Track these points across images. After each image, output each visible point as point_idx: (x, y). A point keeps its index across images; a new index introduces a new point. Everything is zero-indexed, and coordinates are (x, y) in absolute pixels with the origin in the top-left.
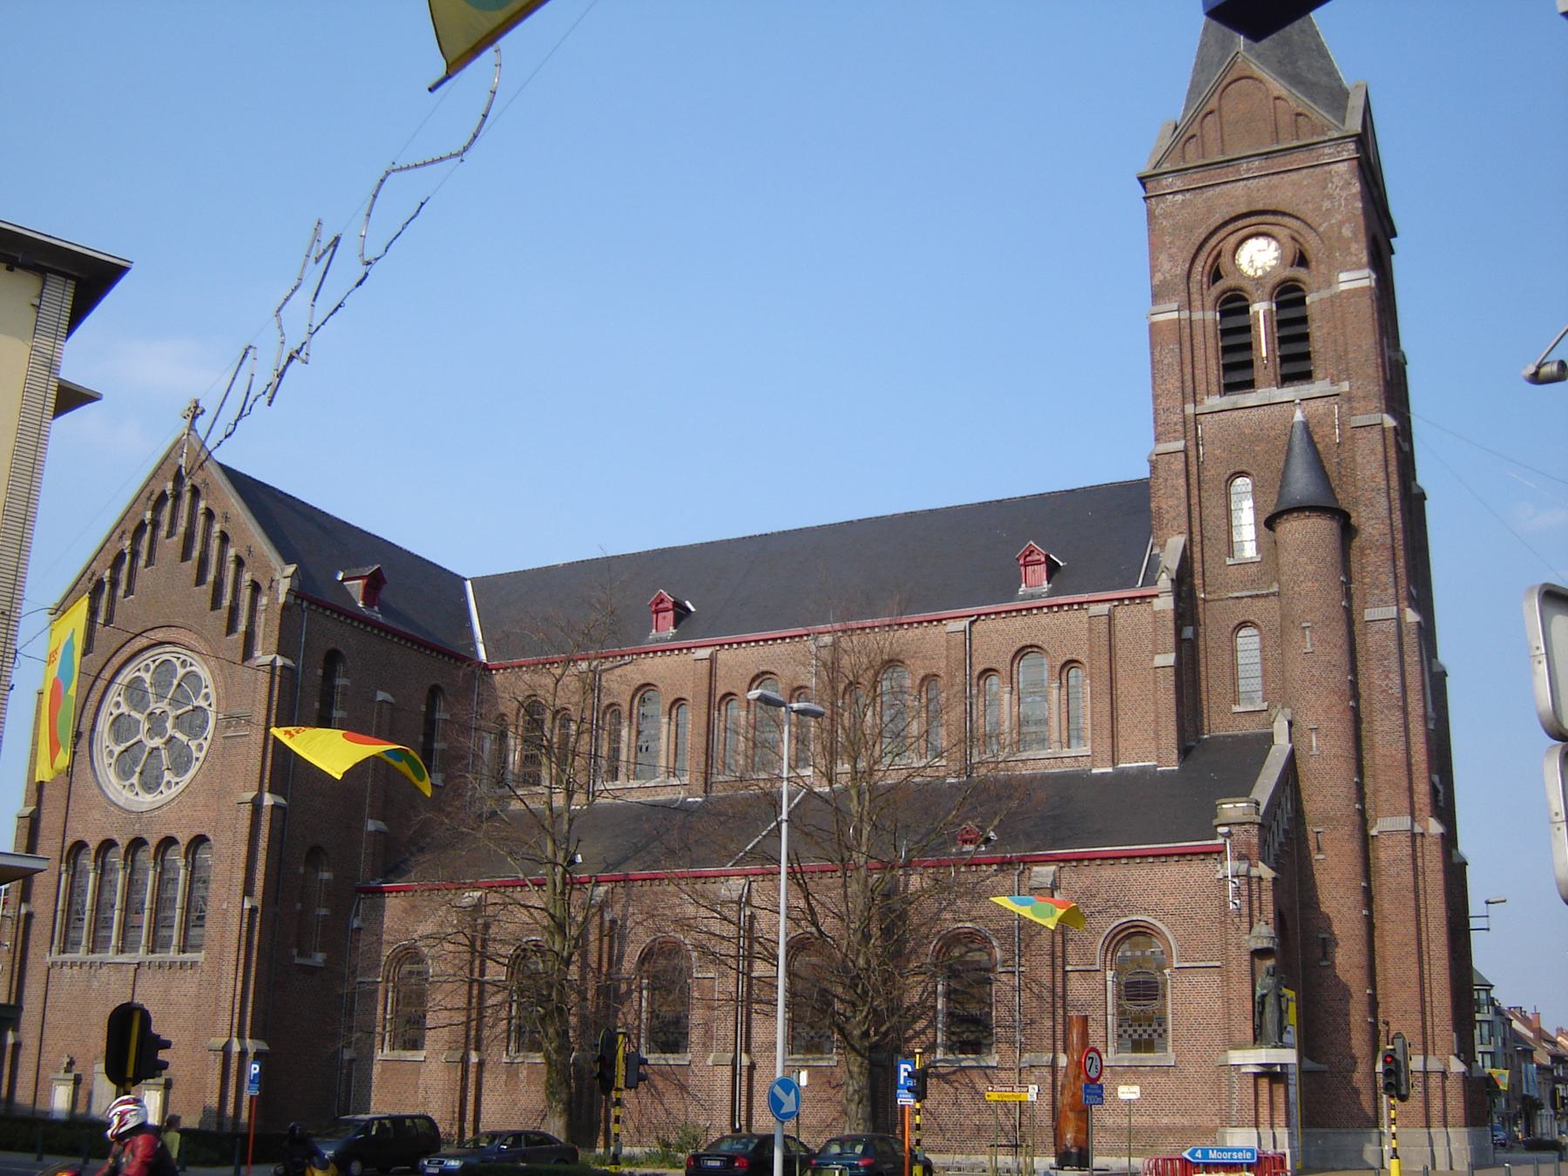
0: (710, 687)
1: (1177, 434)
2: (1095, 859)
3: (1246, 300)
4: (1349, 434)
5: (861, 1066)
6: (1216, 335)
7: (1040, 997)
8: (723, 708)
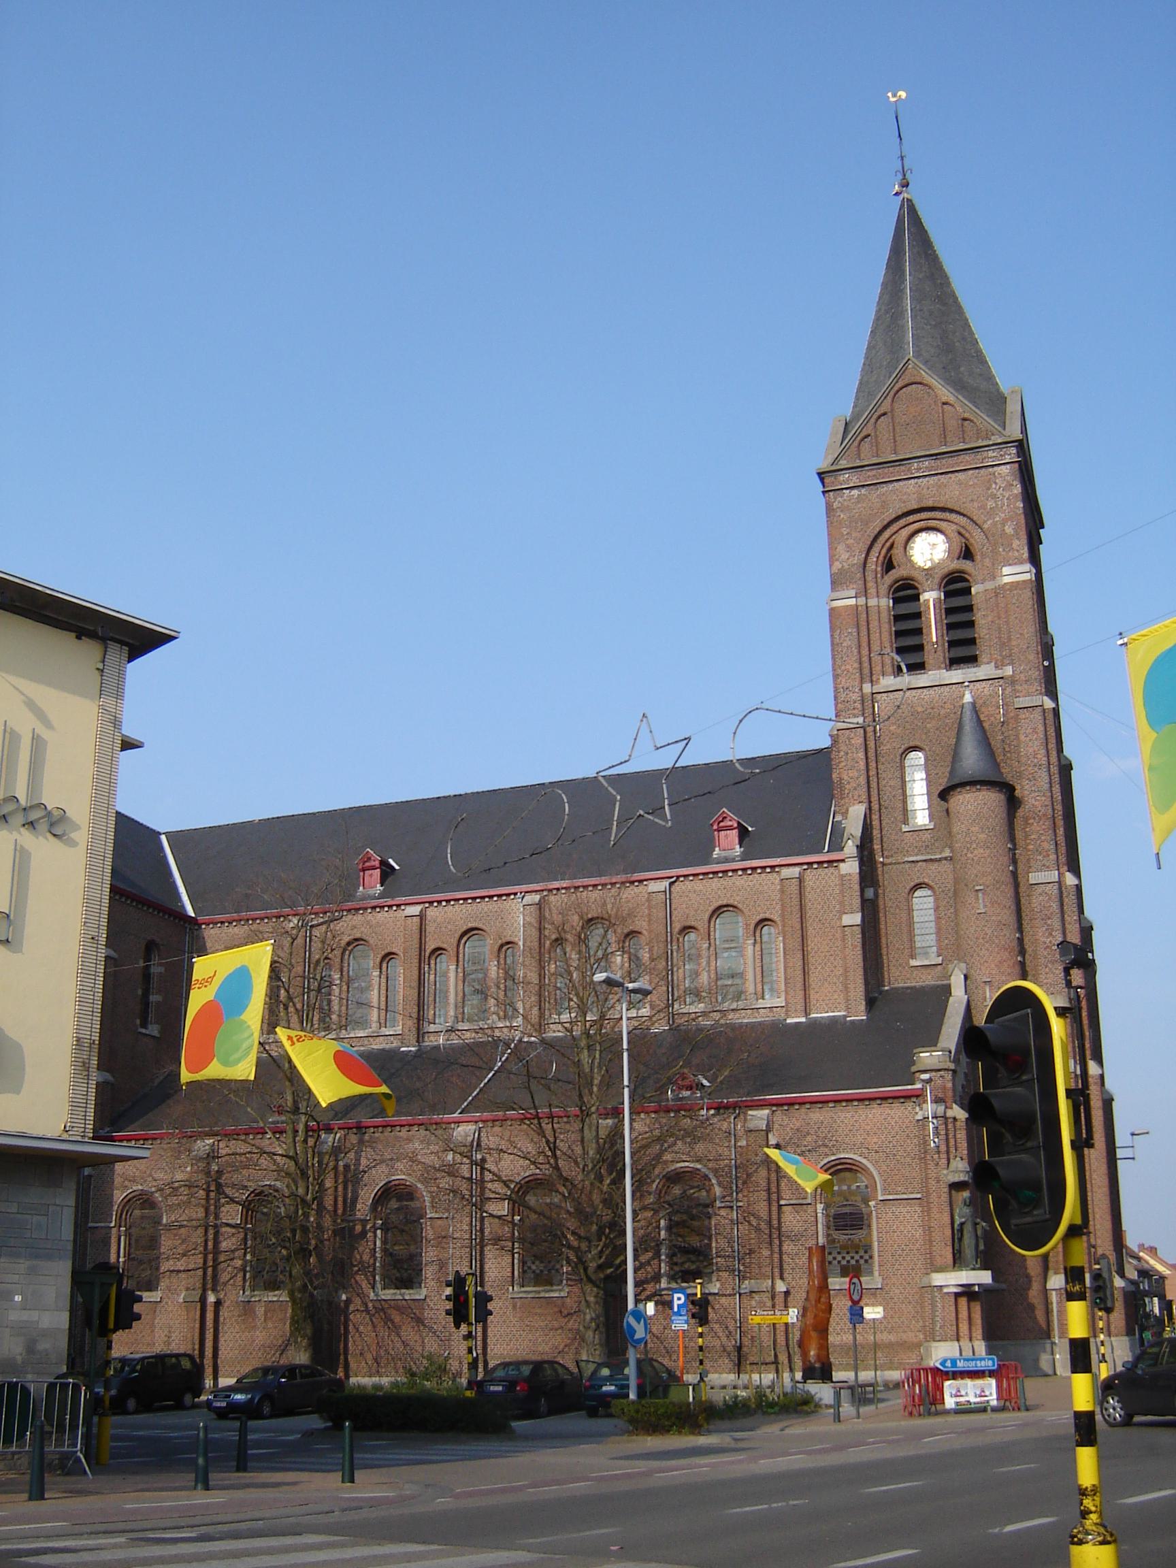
0: (421, 943)
1: (856, 712)
2: (804, 1103)
3: (916, 588)
4: (1012, 714)
5: (596, 1297)
6: (890, 622)
7: (758, 1229)
8: (432, 962)
